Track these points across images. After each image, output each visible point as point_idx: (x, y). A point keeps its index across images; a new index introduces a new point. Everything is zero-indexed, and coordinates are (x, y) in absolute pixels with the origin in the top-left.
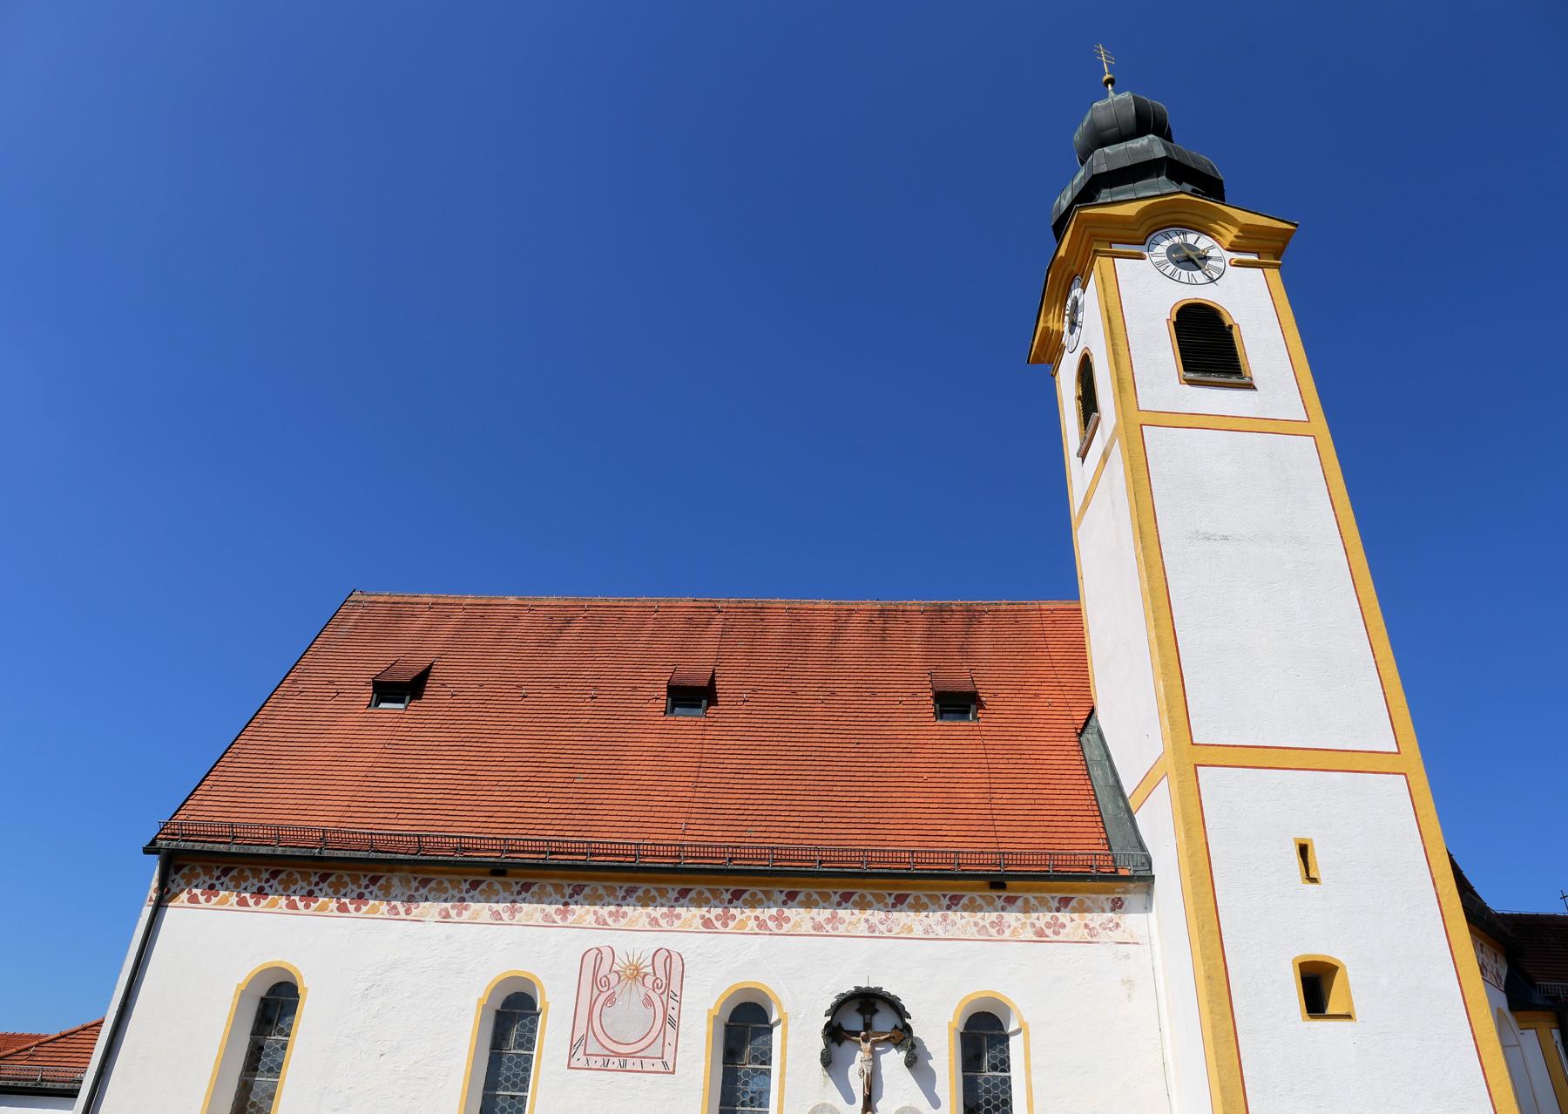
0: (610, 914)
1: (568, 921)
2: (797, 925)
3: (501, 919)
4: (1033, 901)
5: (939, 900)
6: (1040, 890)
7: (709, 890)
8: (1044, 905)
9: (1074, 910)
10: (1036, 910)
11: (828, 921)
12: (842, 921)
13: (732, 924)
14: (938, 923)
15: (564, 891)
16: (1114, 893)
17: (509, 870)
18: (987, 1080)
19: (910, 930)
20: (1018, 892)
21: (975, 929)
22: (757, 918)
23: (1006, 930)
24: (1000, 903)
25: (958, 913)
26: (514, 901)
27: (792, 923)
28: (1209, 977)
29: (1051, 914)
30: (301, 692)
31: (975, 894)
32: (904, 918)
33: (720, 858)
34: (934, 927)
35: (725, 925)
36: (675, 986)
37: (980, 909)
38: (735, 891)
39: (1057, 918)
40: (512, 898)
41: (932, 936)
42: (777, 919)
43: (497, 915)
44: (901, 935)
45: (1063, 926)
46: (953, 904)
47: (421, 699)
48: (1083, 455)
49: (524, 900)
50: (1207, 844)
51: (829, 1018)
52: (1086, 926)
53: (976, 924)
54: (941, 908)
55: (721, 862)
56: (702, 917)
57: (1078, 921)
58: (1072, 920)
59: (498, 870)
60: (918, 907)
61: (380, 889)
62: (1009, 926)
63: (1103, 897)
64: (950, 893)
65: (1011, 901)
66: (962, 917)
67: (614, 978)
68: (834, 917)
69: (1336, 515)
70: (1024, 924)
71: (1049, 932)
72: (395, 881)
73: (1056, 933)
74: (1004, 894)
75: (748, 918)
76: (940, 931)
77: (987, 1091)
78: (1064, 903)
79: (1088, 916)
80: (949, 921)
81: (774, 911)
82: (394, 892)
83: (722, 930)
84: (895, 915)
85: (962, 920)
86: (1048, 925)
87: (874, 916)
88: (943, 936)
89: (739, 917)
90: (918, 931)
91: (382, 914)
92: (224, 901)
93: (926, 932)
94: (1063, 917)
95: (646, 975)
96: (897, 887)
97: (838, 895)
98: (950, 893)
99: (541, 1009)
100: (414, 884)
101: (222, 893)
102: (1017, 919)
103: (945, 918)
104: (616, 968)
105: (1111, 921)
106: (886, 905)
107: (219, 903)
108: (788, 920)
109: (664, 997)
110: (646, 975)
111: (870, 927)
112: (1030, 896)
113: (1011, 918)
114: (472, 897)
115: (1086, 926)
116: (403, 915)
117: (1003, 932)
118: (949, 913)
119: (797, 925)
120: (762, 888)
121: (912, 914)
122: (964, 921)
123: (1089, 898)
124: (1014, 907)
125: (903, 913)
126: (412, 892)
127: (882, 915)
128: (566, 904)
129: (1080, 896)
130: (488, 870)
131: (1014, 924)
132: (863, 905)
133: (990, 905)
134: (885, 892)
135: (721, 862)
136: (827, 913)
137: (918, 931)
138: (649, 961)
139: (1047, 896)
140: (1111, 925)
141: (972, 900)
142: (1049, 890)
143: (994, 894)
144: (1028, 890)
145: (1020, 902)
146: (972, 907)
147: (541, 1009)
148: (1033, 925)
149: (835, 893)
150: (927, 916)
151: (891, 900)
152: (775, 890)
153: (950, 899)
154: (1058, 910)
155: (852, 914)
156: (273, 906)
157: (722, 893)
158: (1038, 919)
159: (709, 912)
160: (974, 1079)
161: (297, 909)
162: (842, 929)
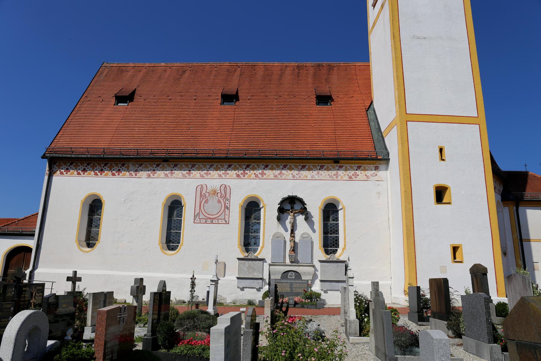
0: (205, 173)
1: (301, 177)
2: (269, 176)
3: (168, 176)
4: (348, 167)
5: (317, 167)
6: (351, 163)
7: (238, 165)
8: (352, 169)
9: (362, 170)
10: (349, 170)
11: (279, 174)
12: (284, 174)
13: (246, 176)
14: (316, 175)
15: (207, 167)
16: (376, 164)
17: (340, 161)
18: (331, 224)
19: (307, 177)
20: (344, 164)
21: (328, 176)
22: (255, 174)
23: (339, 177)
24: (337, 168)
25: (323, 171)
26: (172, 170)
27: (267, 175)
28: (405, 191)
29: (354, 171)
30: (89, 100)
31: (329, 165)
32: (304, 173)
33: (242, 154)
34: (315, 176)
35: (244, 176)
36: (228, 196)
37: (330, 170)
38: (284, 165)
39: (356, 173)
40: (153, 169)
41: (314, 179)
42: (262, 174)
43: (166, 175)
44: (303, 179)
45: (358, 175)
46: (322, 168)
47: (133, 102)
48: (374, 5)
49: (175, 170)
50: (408, 148)
51: (279, 206)
52: (366, 175)
53: (329, 175)
54: (317, 170)
55: (242, 155)
56: (236, 174)
57: (363, 173)
58: (361, 173)
59: (166, 160)
60: (309, 169)
61: (125, 168)
62: (340, 175)
63: (372, 166)
64: (320, 165)
65: (341, 167)
66: (324, 172)
67: (207, 194)
68: (281, 173)
69: (467, 29)
70: (345, 175)
71: (353, 177)
72: (130, 165)
73: (356, 178)
74: (339, 165)
75: (252, 174)
76: (317, 177)
77: (331, 227)
78: (359, 168)
79: (367, 172)
80: (320, 174)
81: (260, 171)
82: (130, 168)
83: (243, 178)
84: (302, 172)
85: (324, 173)
86: (353, 175)
87: (295, 172)
88: (318, 179)
89: (249, 173)
90: (309, 177)
91: (127, 176)
92: (72, 173)
93: (312, 177)
94: (358, 172)
95: (218, 193)
96: (302, 163)
97: (282, 166)
98: (320, 165)
99: (184, 205)
100: (137, 166)
101: (106, 172)
102: (343, 173)
103: (318, 173)
104: (208, 191)
105: (374, 174)
106: (299, 169)
107: (71, 174)
108: (265, 174)
109: (224, 200)
110: (218, 193)
111: (293, 176)
112: (347, 165)
113: (341, 173)
114: (157, 169)
115: (366, 175)
116: (134, 176)
117: (338, 177)
118: (320, 171)
119: (269, 176)
120: (238, 164)
121: (307, 172)
122: (325, 174)
123: (367, 166)
124: (342, 169)
125: (304, 171)
126: (137, 168)
127: (297, 172)
128: (190, 171)
129: (364, 165)
130: (162, 160)
131: (342, 175)
132: (291, 169)
133: (334, 169)
134: (298, 165)
135: (242, 155)
136: (278, 172)
137: (309, 177)
138: (219, 189)
139: (353, 165)
140: (374, 175)
141: (328, 167)
142: (354, 163)
143: (335, 165)
144: (347, 163)
145: (344, 168)
146: (328, 169)
147: (184, 205)
148: (348, 175)
149: (281, 165)
150: (312, 172)
151: (300, 167)
152: (261, 164)
153: (320, 167)
154: (357, 170)
155: (287, 172)
156: (90, 175)
157: (243, 166)
158: (350, 173)
159: (331, 173)
160: (327, 224)
161: (64, 174)
162: (283, 177)
